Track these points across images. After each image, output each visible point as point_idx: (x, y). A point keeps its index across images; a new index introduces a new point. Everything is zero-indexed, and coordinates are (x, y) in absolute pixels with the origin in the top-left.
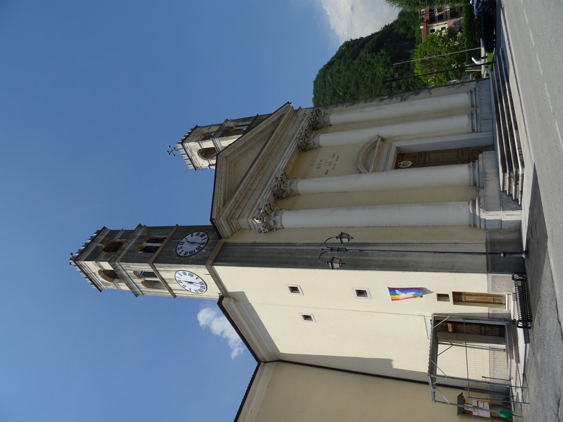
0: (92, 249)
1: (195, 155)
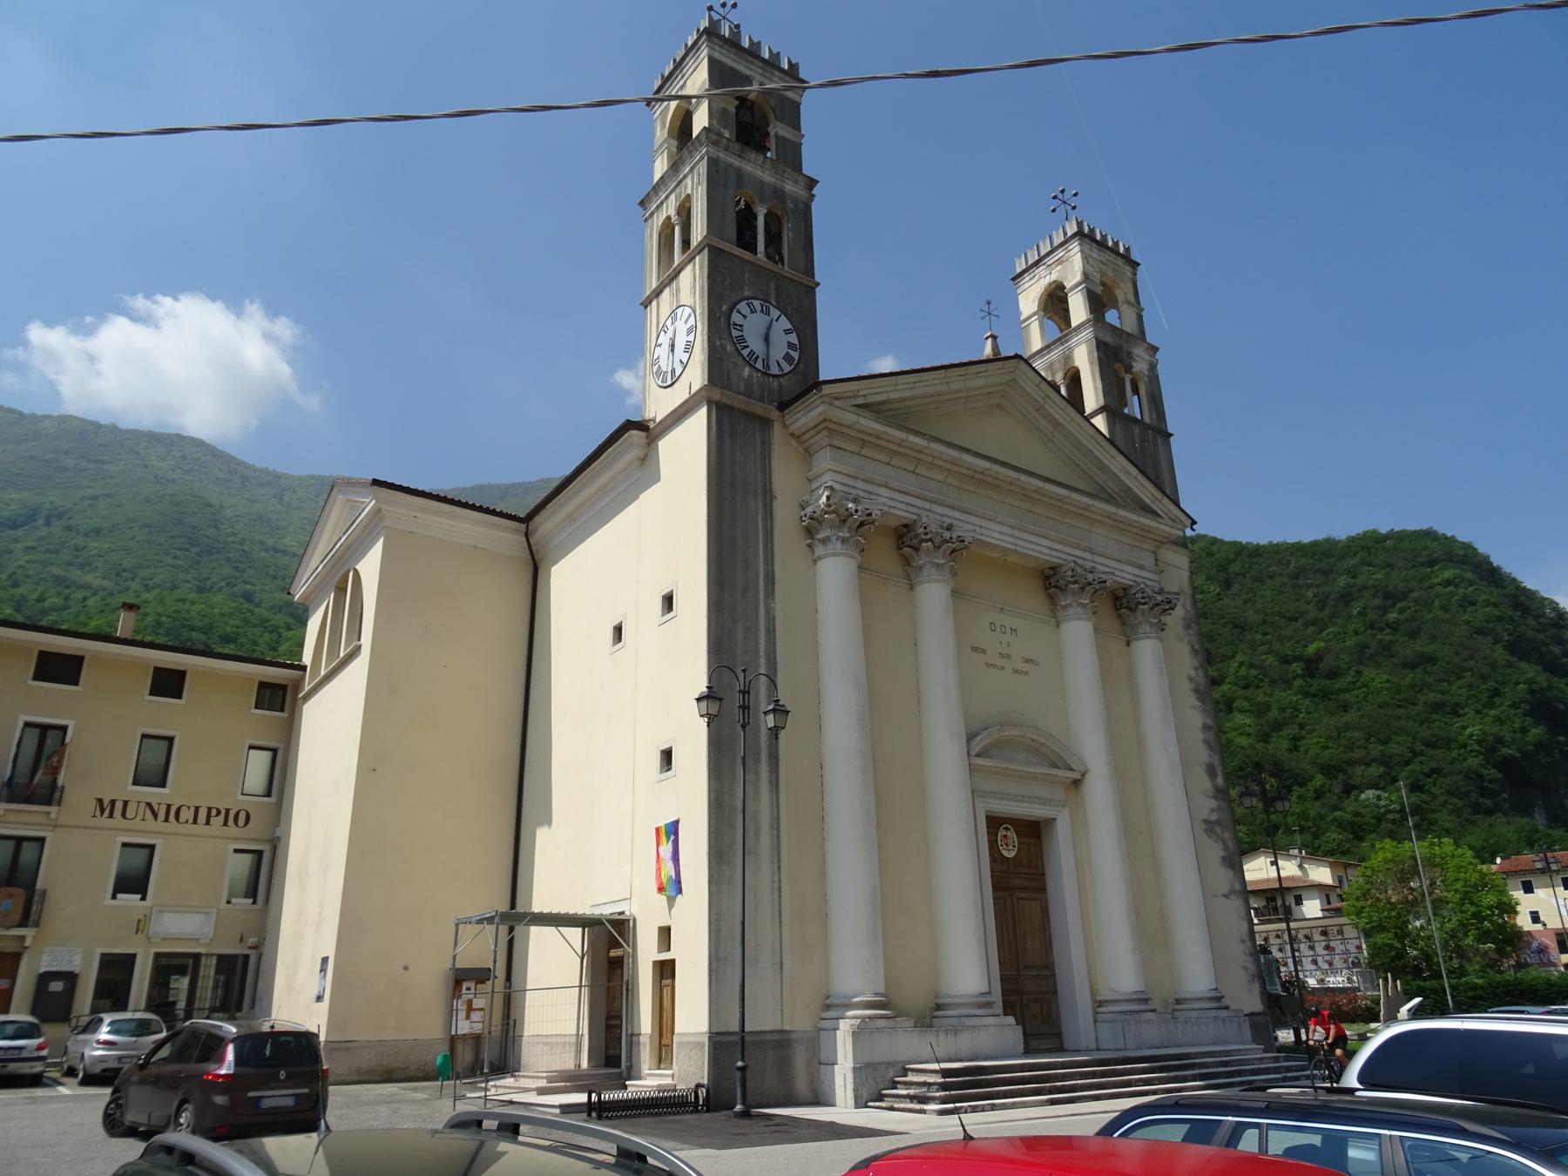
0: (743, 68)
1: (1051, 274)
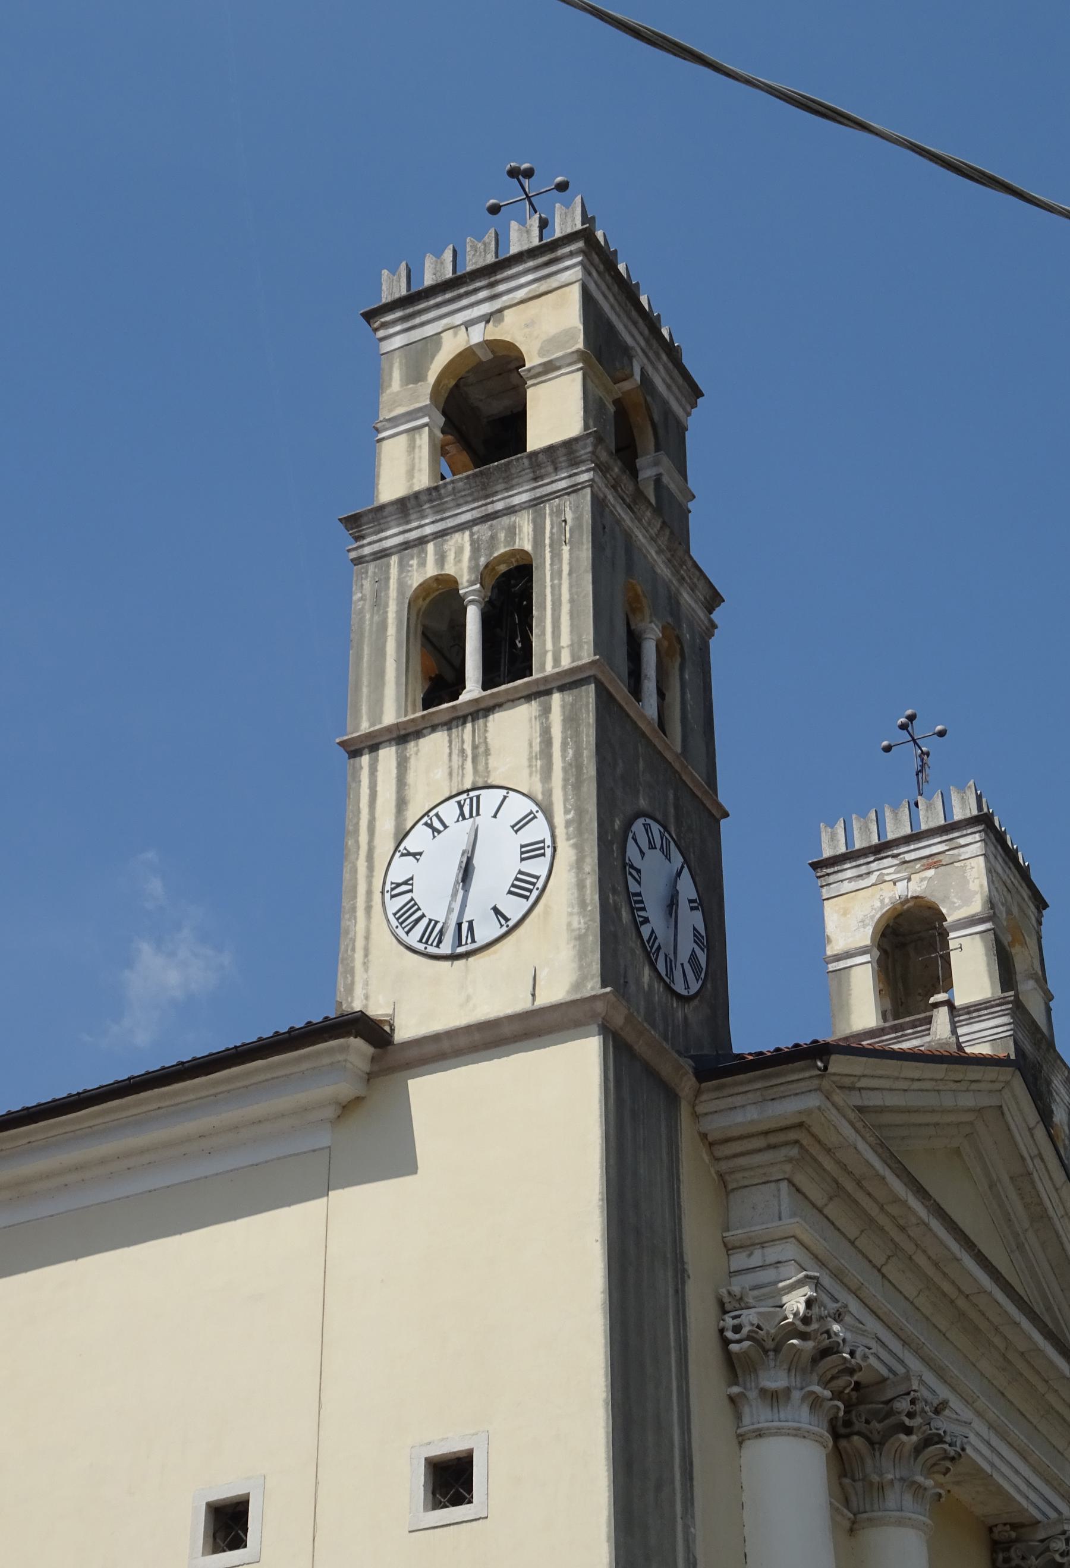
1: (909, 879)
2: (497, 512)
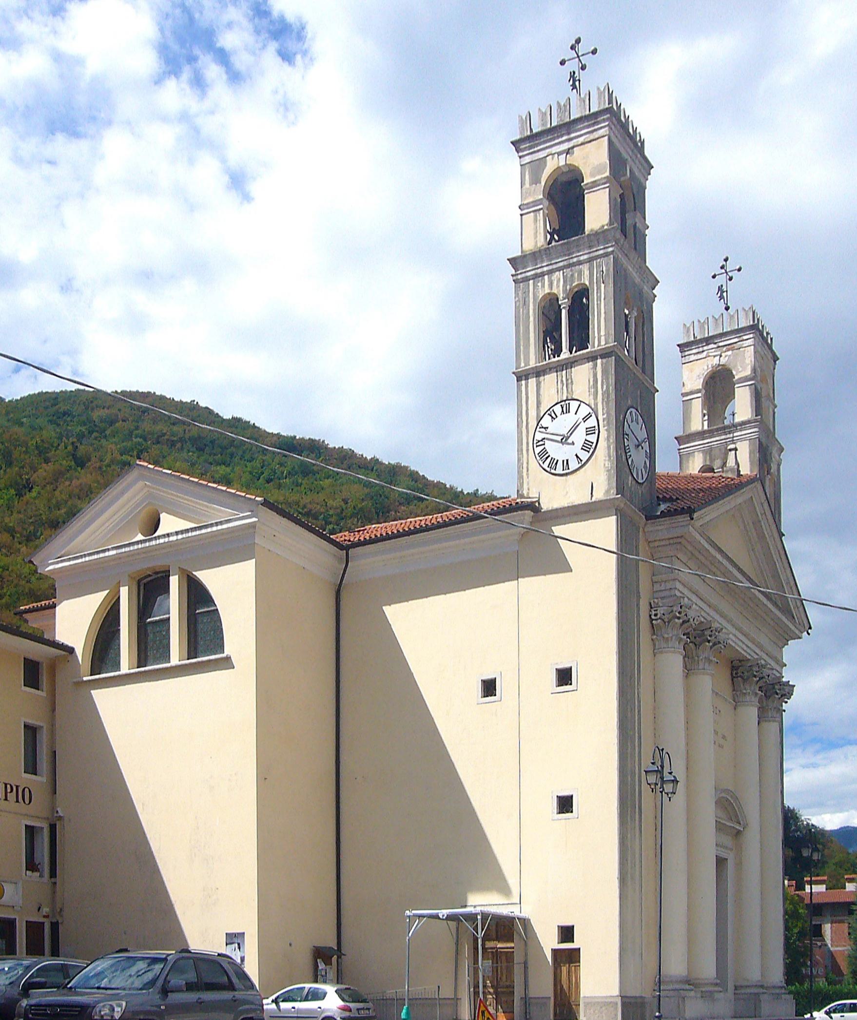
1: (721, 356)
2: (574, 263)
